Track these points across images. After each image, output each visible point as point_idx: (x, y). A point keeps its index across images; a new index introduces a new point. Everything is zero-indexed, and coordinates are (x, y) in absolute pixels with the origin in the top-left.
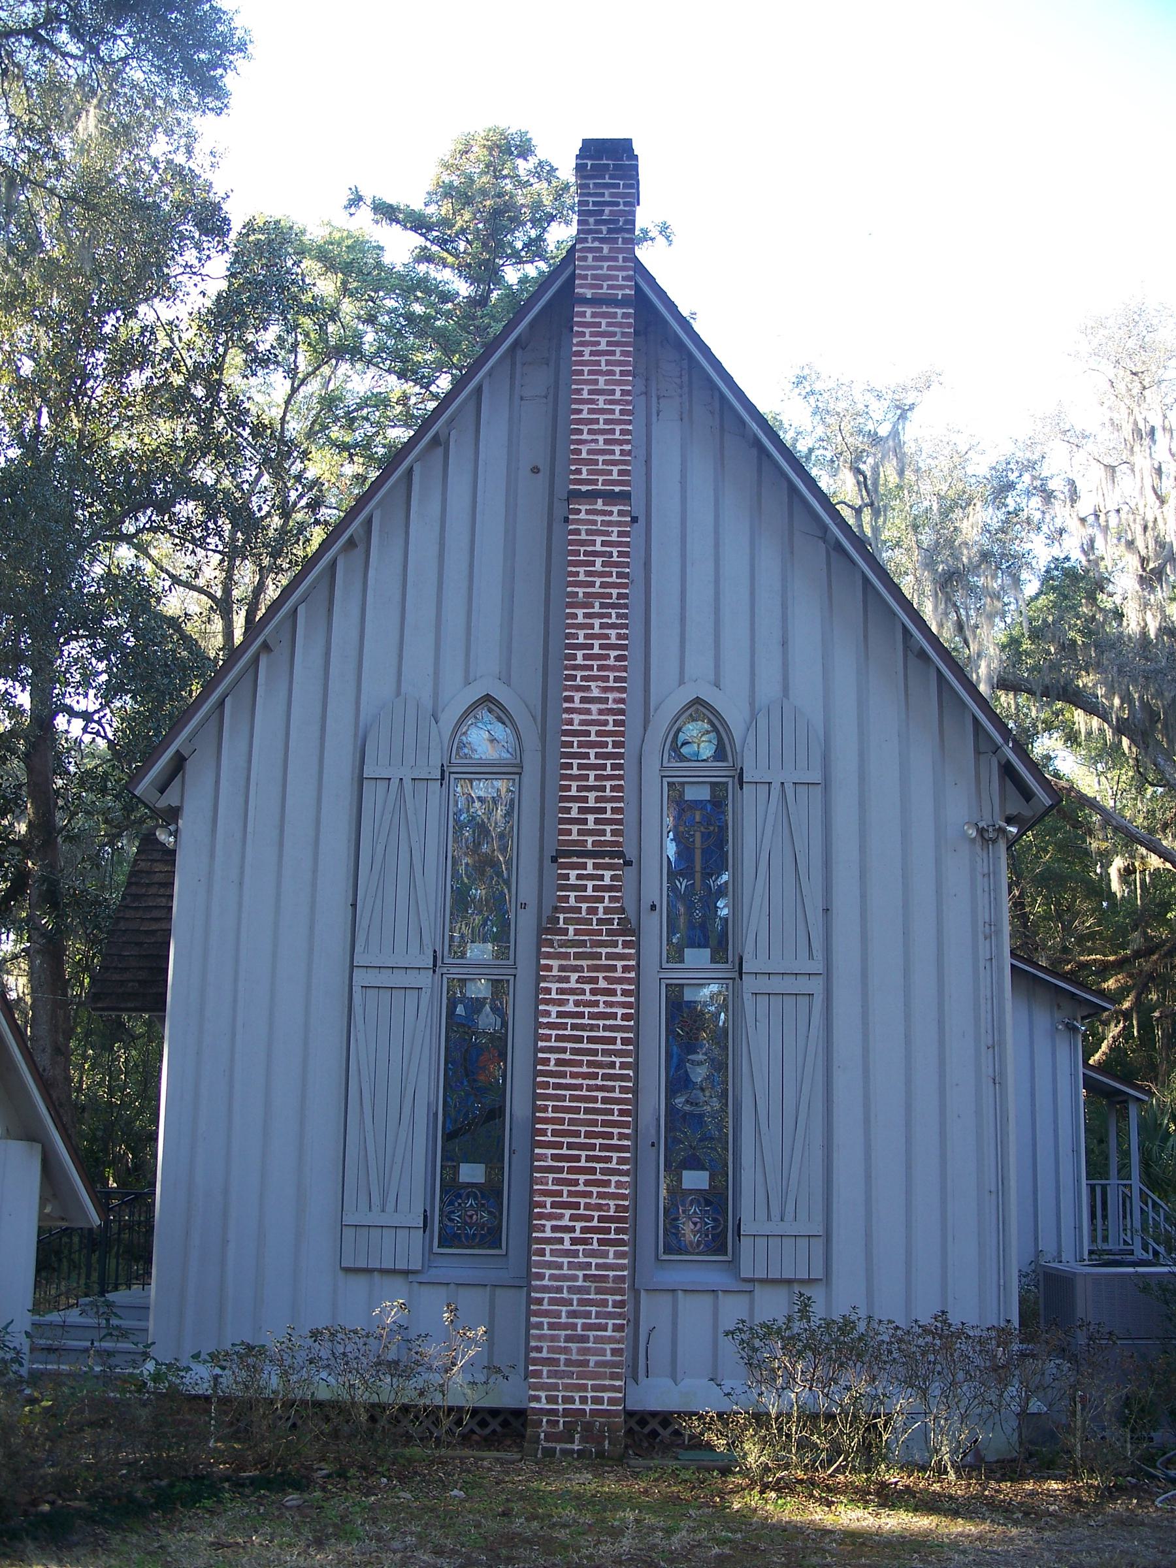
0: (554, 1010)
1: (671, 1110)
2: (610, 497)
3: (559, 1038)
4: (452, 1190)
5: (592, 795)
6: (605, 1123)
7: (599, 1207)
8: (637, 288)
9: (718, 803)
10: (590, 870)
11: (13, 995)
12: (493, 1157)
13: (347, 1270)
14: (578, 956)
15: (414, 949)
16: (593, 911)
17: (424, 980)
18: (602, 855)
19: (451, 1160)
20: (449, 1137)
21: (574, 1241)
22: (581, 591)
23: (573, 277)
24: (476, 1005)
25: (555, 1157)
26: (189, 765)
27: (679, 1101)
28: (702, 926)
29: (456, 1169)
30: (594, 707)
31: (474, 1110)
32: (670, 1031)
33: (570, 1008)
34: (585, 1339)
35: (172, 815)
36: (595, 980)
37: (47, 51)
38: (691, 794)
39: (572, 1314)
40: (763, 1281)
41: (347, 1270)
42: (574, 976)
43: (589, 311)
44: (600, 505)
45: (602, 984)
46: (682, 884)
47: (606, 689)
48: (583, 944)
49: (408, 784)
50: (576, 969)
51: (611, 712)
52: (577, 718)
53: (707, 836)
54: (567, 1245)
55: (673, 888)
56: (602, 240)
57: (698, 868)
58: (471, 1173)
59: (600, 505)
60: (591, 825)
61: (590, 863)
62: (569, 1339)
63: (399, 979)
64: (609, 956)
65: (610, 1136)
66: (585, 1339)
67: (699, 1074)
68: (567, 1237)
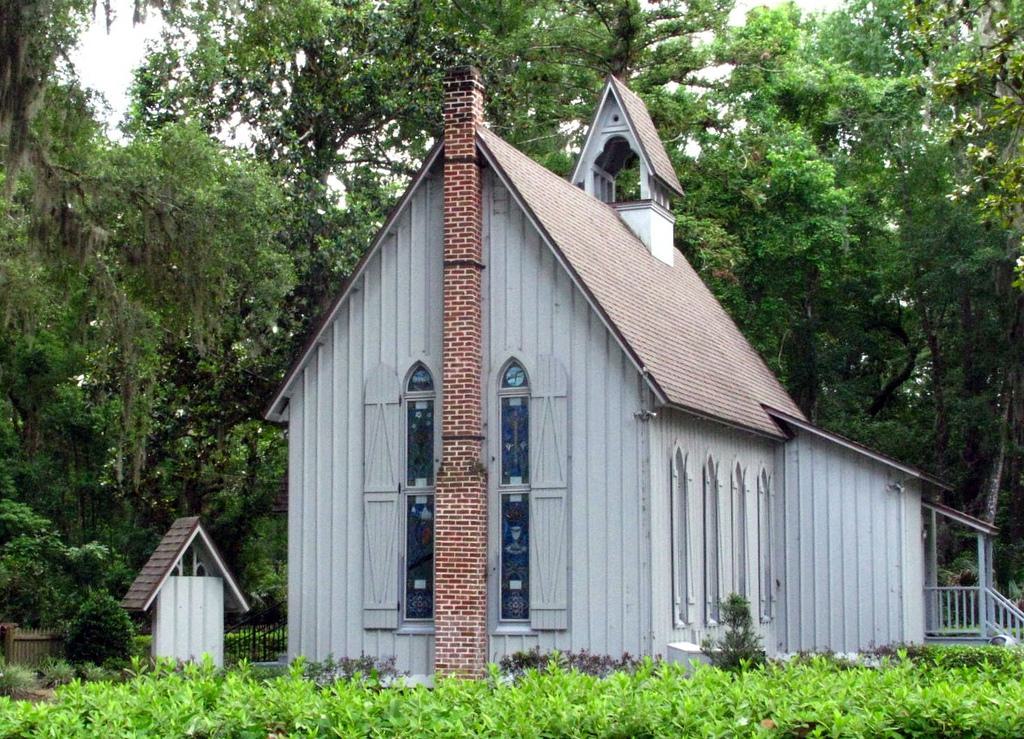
0: (442, 510)
1: (504, 553)
2: (463, 264)
3: (445, 523)
4: (411, 591)
5: (457, 411)
6: (465, 560)
7: (463, 598)
8: (479, 152)
9: (525, 407)
10: (457, 445)
11: (1016, 269)
12: (429, 577)
13: (369, 630)
14: (452, 485)
15: (390, 484)
16: (458, 464)
17: (394, 497)
18: (461, 438)
19: (411, 580)
20: (410, 568)
21: (453, 613)
22: (450, 312)
23: (442, 153)
24: (420, 507)
25: (444, 576)
26: (291, 402)
27: (508, 548)
28: (517, 464)
29: (413, 584)
30: (457, 369)
31: (420, 559)
32: (504, 516)
33: (449, 509)
34: (457, 656)
35: (285, 425)
36: (459, 496)
37: (9, 545)
38: (513, 403)
39: (452, 645)
40: (543, 631)
41: (369, 630)
42: (450, 494)
43: (451, 166)
44: (458, 268)
45: (462, 497)
46: (509, 447)
47: (462, 360)
48: (453, 479)
49: (385, 407)
50: (452, 491)
51: (465, 370)
52: (450, 374)
53: (516, 423)
54: (450, 614)
55: (504, 449)
56: (457, 126)
57: (516, 438)
58: (420, 584)
59: (458, 268)
60: (457, 425)
61: (457, 442)
62: (451, 656)
63: (384, 497)
64: (466, 485)
65: (466, 566)
66: (457, 656)
67: (516, 536)
68: (449, 611)
